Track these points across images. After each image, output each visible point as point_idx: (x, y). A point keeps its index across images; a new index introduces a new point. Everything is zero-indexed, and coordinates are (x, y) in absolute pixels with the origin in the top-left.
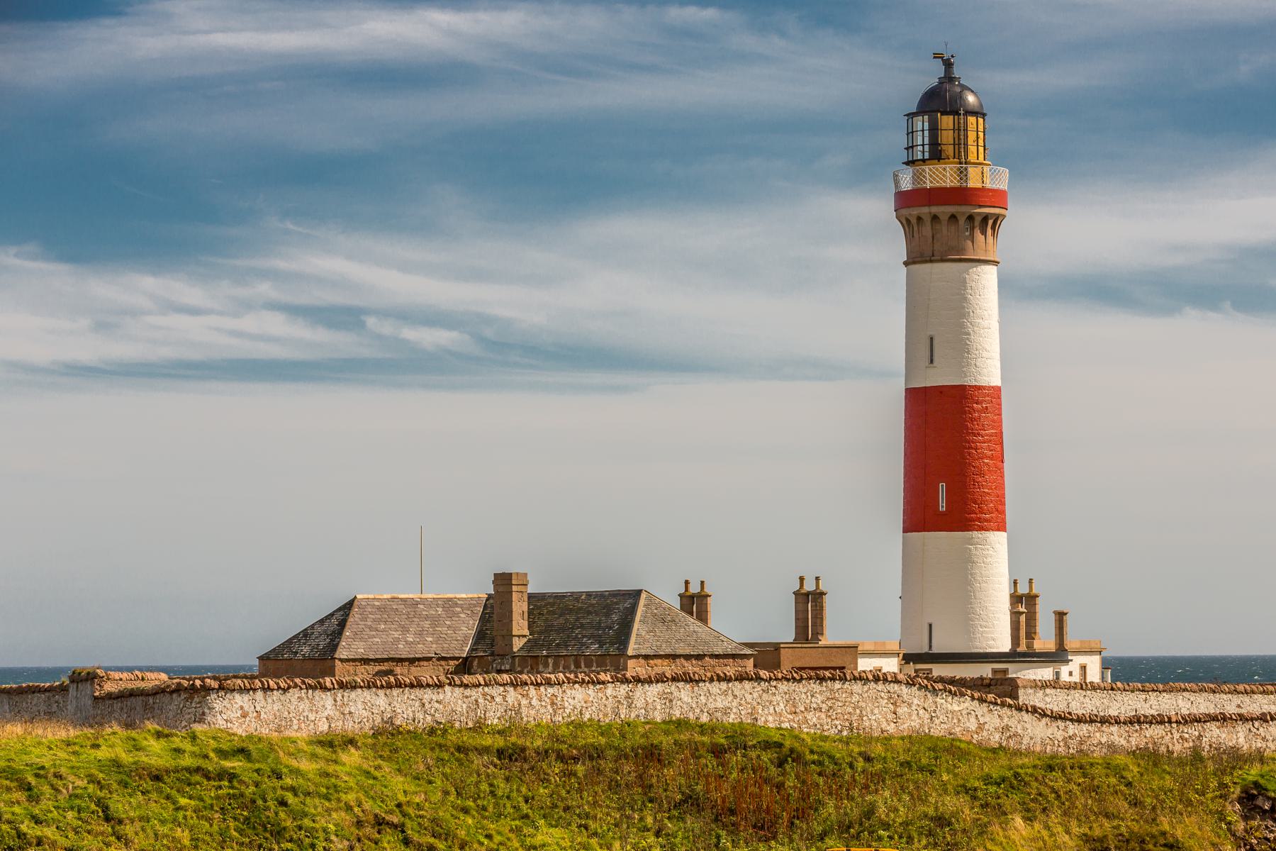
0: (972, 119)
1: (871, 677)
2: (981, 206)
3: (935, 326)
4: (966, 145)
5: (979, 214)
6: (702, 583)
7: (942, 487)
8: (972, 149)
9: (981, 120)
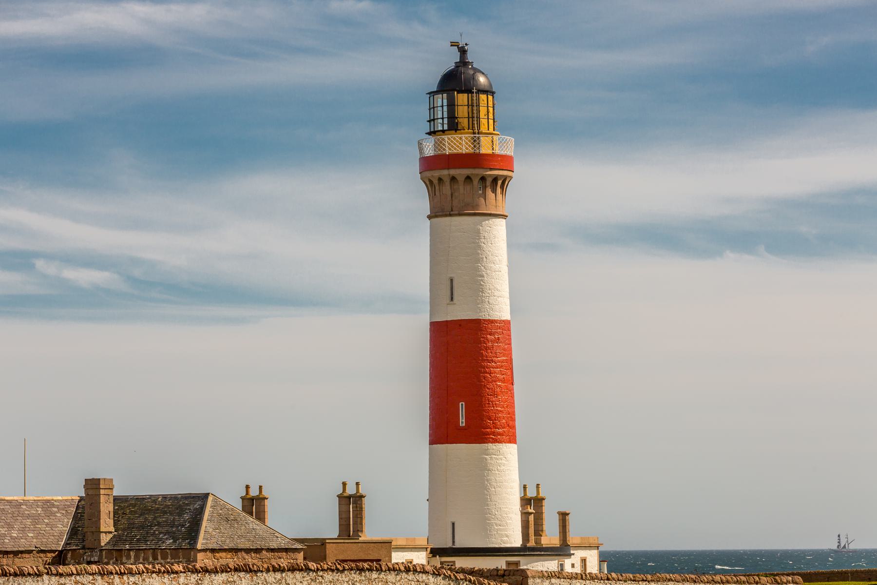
0: (483, 97)
1: (402, 568)
2: (491, 169)
3: (455, 270)
6: (260, 487)
7: (462, 405)
8: (484, 121)
9: (490, 97)
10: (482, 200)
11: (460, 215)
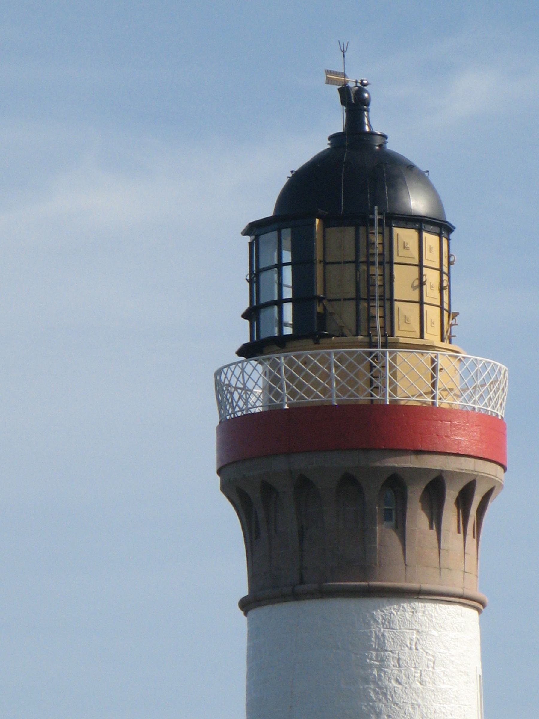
0: (405, 236)
2: (419, 452)
4: (388, 300)
5: (456, 475)
8: (405, 313)
9: (445, 241)
10: (393, 537)
11: (324, 594)
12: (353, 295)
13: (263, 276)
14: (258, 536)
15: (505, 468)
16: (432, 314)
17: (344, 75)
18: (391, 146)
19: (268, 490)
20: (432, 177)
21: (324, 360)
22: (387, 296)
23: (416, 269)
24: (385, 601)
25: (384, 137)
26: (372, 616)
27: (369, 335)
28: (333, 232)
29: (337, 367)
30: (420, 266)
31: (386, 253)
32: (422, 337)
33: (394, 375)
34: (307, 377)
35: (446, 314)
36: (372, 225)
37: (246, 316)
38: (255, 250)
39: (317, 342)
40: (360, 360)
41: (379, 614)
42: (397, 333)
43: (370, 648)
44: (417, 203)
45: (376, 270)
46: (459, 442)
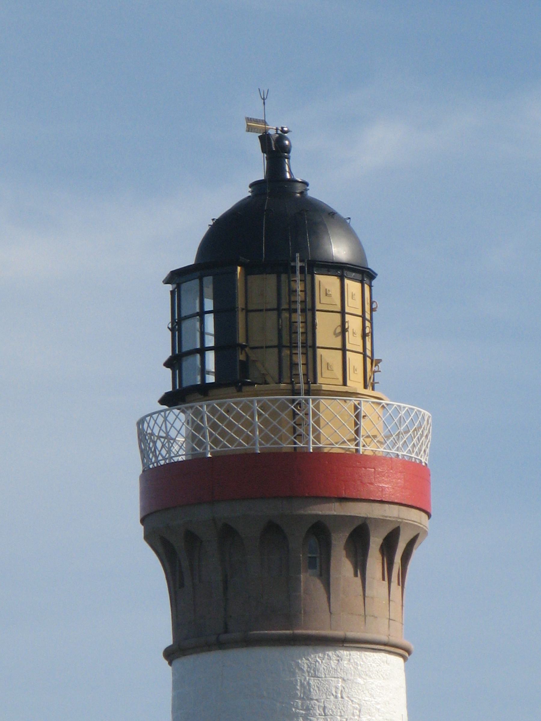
0: (327, 283)
2: (328, 499)
4: (311, 347)
5: (383, 522)
8: (328, 359)
9: (367, 287)
10: (318, 585)
11: (249, 642)
12: (275, 343)
13: (186, 325)
14: (182, 585)
15: (429, 515)
16: (355, 361)
17: (265, 123)
18: (312, 193)
19: (192, 538)
20: (353, 224)
21: (247, 408)
22: (310, 343)
23: (339, 316)
24: (310, 649)
25: (305, 184)
26: (298, 665)
27: (292, 383)
28: (256, 280)
29: (260, 415)
30: (343, 313)
31: (308, 299)
32: (345, 383)
33: (318, 422)
34: (230, 425)
35: (368, 361)
36: (294, 272)
37: (168, 364)
38: (176, 298)
39: (239, 390)
40: (283, 407)
41: (304, 663)
42: (320, 380)
43: (295, 696)
44: (339, 250)
45: (298, 318)
46: (383, 489)
